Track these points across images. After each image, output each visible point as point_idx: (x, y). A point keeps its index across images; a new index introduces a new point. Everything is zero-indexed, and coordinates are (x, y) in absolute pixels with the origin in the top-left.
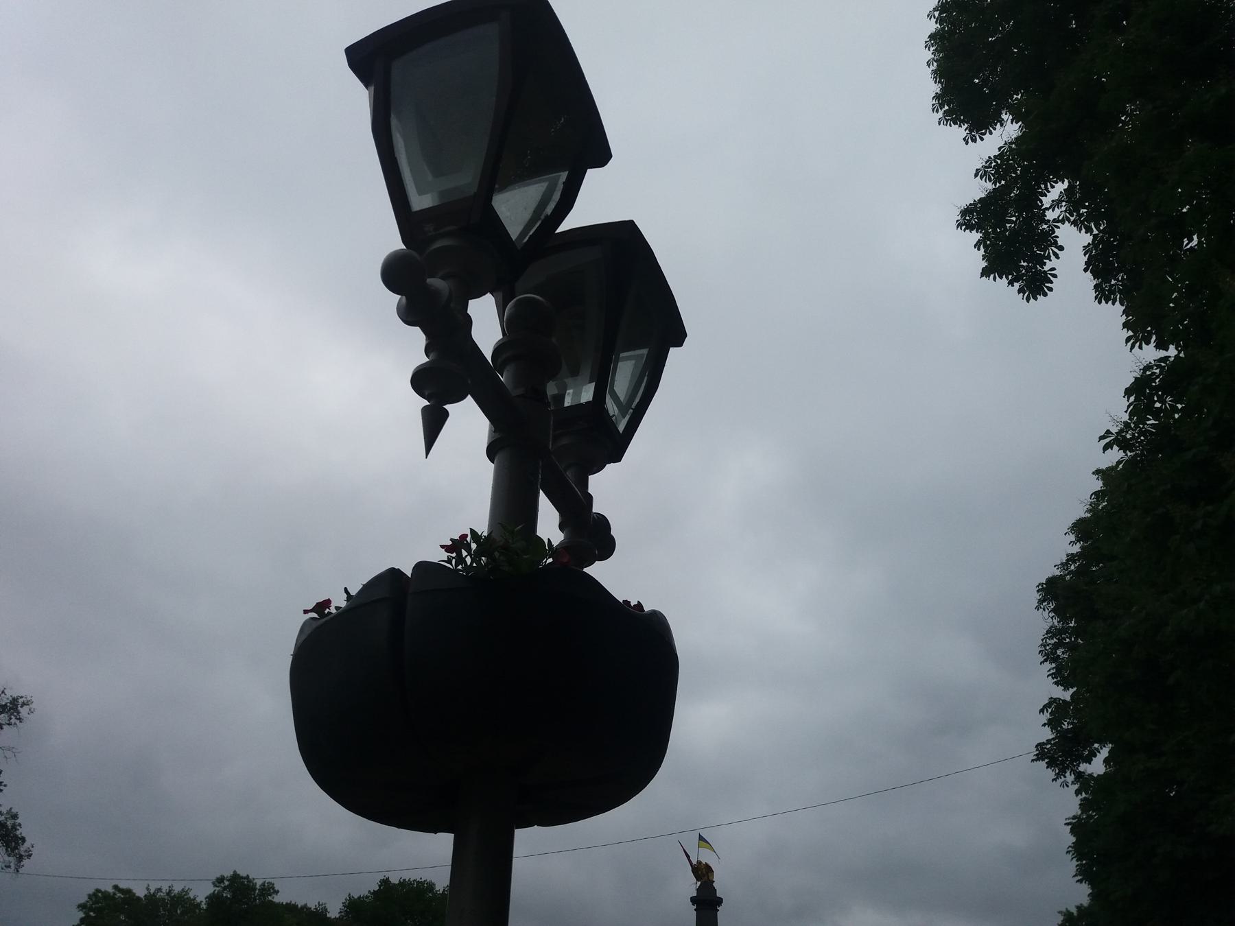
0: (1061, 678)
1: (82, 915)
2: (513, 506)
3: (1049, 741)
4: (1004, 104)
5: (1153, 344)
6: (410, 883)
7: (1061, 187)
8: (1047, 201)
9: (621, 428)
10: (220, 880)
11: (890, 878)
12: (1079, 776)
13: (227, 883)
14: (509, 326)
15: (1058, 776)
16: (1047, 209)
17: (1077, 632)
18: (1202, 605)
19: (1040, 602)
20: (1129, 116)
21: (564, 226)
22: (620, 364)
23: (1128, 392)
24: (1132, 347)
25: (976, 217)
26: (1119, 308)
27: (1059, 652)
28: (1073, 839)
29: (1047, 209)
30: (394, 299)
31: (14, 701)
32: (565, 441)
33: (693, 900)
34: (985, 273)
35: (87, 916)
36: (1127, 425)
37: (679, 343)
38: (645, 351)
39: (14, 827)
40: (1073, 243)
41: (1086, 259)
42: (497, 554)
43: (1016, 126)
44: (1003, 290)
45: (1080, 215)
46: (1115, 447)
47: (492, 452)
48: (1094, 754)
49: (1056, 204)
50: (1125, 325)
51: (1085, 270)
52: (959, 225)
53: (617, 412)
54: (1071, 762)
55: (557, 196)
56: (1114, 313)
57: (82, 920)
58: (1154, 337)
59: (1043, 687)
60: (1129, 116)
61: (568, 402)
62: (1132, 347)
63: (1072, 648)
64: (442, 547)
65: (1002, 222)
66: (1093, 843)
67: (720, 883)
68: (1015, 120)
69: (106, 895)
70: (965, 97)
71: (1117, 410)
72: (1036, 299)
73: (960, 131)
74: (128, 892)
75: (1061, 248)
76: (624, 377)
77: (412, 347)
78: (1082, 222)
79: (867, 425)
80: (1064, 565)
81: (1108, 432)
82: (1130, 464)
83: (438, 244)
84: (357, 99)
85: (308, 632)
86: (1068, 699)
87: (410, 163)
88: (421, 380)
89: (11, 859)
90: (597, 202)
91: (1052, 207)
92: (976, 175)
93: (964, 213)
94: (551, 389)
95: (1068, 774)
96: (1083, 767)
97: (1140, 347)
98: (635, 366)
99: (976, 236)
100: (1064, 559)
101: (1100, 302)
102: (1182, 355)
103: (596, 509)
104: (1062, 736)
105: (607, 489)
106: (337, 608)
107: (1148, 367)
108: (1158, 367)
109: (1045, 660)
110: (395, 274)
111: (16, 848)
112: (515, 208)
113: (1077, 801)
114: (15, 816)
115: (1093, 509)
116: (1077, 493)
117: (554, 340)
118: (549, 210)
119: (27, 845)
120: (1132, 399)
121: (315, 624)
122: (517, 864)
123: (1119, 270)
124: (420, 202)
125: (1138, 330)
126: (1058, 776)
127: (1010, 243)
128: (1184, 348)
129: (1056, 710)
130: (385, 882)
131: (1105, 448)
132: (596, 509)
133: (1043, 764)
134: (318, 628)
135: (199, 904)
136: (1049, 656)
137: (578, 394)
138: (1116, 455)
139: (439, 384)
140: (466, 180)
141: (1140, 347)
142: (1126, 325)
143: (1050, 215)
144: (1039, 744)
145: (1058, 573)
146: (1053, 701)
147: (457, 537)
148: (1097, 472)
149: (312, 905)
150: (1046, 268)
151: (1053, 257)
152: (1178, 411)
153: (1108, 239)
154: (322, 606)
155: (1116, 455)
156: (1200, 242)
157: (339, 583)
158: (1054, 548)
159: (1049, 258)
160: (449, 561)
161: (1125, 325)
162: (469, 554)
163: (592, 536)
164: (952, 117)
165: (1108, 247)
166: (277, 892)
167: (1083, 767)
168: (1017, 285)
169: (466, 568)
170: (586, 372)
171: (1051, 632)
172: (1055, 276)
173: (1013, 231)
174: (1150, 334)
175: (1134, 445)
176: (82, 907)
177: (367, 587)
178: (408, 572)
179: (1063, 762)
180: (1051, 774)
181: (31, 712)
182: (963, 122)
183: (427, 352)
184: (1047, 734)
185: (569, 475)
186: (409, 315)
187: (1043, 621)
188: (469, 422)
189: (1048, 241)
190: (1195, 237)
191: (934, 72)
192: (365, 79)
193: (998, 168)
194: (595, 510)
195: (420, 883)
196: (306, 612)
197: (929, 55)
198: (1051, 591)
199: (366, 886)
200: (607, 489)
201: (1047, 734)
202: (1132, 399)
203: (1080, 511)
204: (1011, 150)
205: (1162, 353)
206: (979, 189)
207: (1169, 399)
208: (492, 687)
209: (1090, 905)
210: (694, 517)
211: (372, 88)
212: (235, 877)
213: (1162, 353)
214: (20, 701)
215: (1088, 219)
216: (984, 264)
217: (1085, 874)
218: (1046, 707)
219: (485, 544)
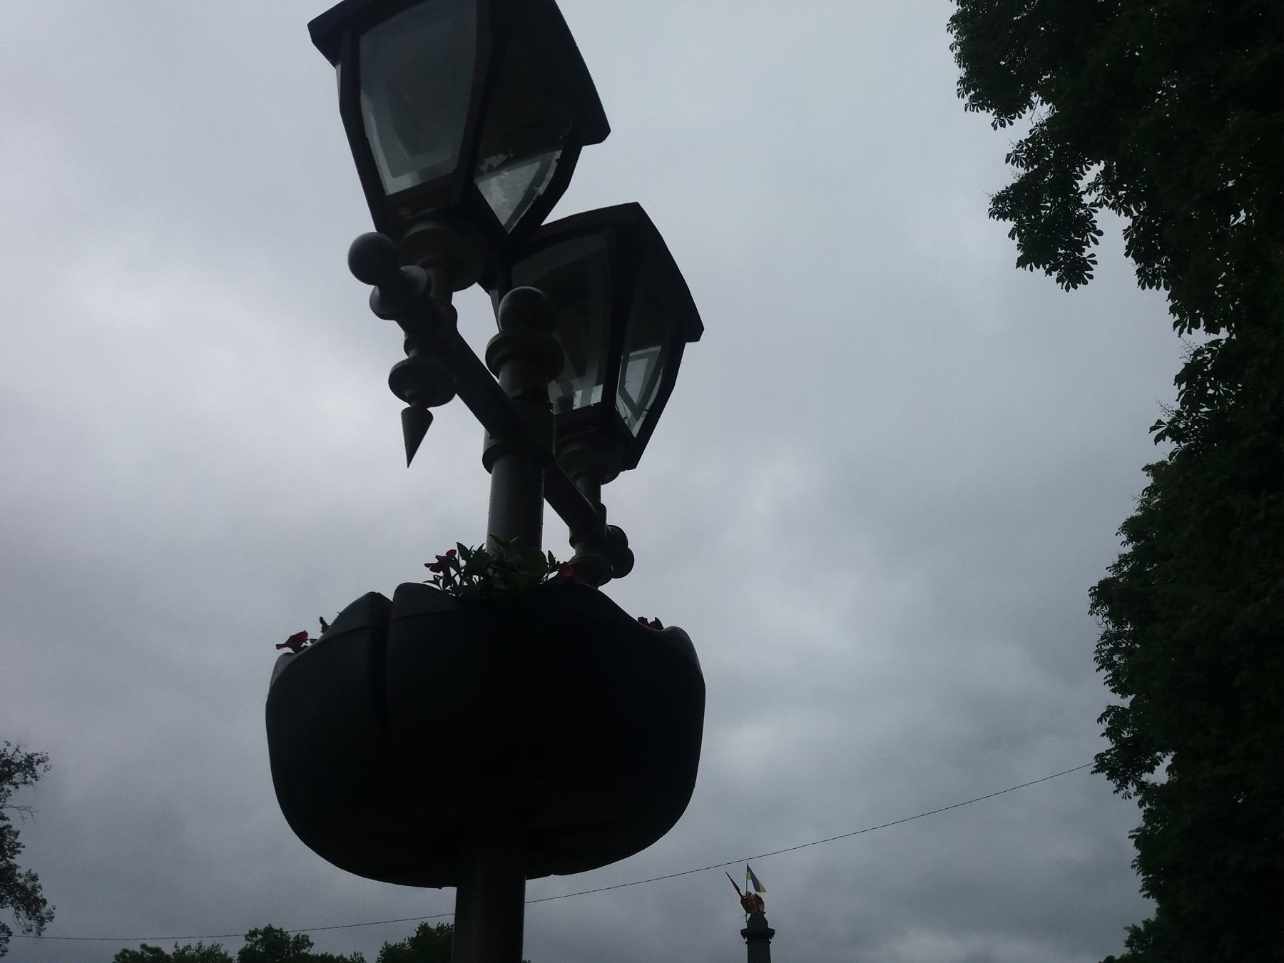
0: (1119, 684)
2: (515, 519)
3: (1108, 752)
4: (1032, 86)
5: (1202, 327)
7: (1097, 169)
8: (1082, 184)
9: (635, 432)
10: (253, 934)
11: (951, 900)
12: (1142, 786)
13: (260, 937)
14: (505, 320)
15: (1120, 787)
16: (1084, 193)
17: (1133, 636)
19: (1093, 606)
20: (1168, 88)
21: (558, 213)
22: (630, 364)
23: (1179, 379)
24: (1181, 332)
26: (1164, 293)
27: (1115, 658)
28: (1139, 853)
29: (1084, 193)
30: (366, 291)
31: (29, 758)
32: (572, 448)
33: (744, 933)
34: (1021, 263)
36: (1179, 414)
38: (658, 348)
39: (34, 889)
40: (1112, 225)
42: (490, 571)
43: (1046, 107)
44: (1041, 280)
45: (1119, 198)
46: (1168, 439)
48: (1156, 762)
49: (1092, 187)
51: (1127, 255)
52: (992, 214)
53: (629, 414)
54: (1133, 773)
56: (1159, 298)
59: (1101, 695)
60: (1168, 88)
61: (577, 404)
62: (1181, 332)
63: (1128, 653)
64: (427, 565)
65: (1036, 209)
66: (1159, 856)
69: (134, 955)
70: (992, 79)
71: (1169, 398)
73: (988, 116)
74: (157, 950)
75: (1100, 233)
76: (635, 375)
77: (389, 343)
78: (1121, 205)
80: (1117, 567)
81: (1159, 422)
82: (1182, 458)
83: (414, 230)
85: (281, 669)
86: (1127, 706)
87: (386, 153)
88: (400, 381)
89: (32, 922)
90: (594, 184)
91: (1089, 191)
92: (1007, 161)
93: (998, 200)
94: (554, 392)
95: (1130, 785)
96: (1146, 777)
97: (1190, 332)
98: (648, 366)
99: (1010, 224)
100: (1116, 561)
101: (1143, 288)
102: (1234, 337)
103: (610, 521)
104: (1121, 745)
105: (622, 499)
106: (312, 641)
107: (1199, 352)
108: (1210, 351)
109: (1101, 667)
111: (37, 910)
112: (502, 193)
113: (1140, 812)
114: (34, 878)
116: (1128, 493)
118: (541, 190)
119: (49, 906)
120: (1183, 386)
121: (292, 658)
123: (1162, 253)
124: (395, 184)
125: (1188, 311)
126: (1120, 787)
127: (1046, 231)
128: (1236, 331)
129: (1115, 720)
130: (424, 928)
131: (1157, 440)
132: (610, 521)
136: (1105, 663)
137: (586, 396)
138: (1169, 446)
140: (445, 157)
141: (1190, 332)
143: (1087, 199)
145: (1110, 575)
146: (1111, 709)
147: (443, 554)
148: (1147, 468)
150: (1085, 255)
151: (1092, 243)
153: (1149, 221)
154: (297, 640)
155: (1169, 446)
156: (1247, 218)
157: (317, 608)
158: (1106, 549)
159: (1087, 244)
160: (436, 581)
162: (459, 573)
163: (607, 551)
164: (979, 102)
167: (1146, 777)
168: (1055, 274)
169: (457, 588)
170: (593, 373)
171: (1107, 638)
172: (1095, 262)
173: (1047, 217)
175: (1187, 435)
177: (343, 616)
178: (390, 595)
179: (1124, 773)
180: (1112, 785)
182: (991, 106)
183: (407, 348)
184: (1106, 744)
185: (579, 485)
186: (383, 308)
187: (1097, 626)
188: (458, 428)
189: (1085, 226)
190: (1243, 213)
191: (958, 56)
192: (332, 56)
193: (1029, 152)
196: (279, 647)
197: (951, 38)
198: (1104, 594)
200: (622, 499)
201: (1106, 744)
202: (1183, 386)
203: (1131, 508)
205: (1213, 337)
206: (1011, 175)
208: (494, 720)
210: (714, 527)
211: (339, 67)
212: (269, 930)
213: (1213, 337)
214: (36, 758)
215: (1128, 201)
216: (1020, 254)
217: (1151, 888)
219: (476, 560)
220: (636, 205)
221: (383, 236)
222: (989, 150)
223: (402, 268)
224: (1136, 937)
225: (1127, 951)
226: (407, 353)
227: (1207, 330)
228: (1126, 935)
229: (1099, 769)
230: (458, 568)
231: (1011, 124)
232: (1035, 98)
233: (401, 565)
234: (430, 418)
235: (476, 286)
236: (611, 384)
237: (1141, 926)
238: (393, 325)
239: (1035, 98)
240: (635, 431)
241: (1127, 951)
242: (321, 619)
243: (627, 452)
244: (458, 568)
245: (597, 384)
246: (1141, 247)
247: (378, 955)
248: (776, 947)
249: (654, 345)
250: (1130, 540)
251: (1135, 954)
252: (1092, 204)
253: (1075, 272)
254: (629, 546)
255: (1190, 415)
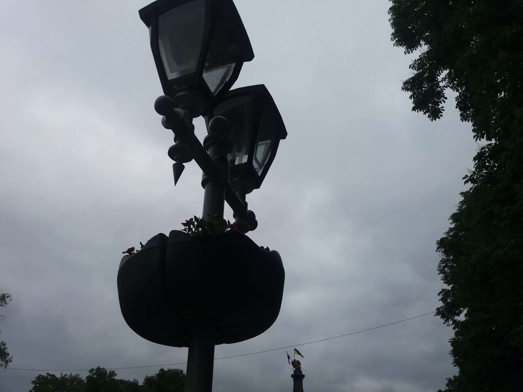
1: (33, 386)
2: (213, 206)
3: (442, 307)
5: (485, 138)
6: (173, 370)
7: (446, 72)
9: (260, 174)
10: (92, 370)
11: (377, 366)
12: (455, 322)
13: (95, 371)
14: (211, 130)
15: (446, 322)
17: (453, 261)
18: (506, 248)
19: (438, 248)
20: (475, 41)
21: (233, 88)
23: (475, 159)
24: (477, 140)
25: (410, 85)
26: (471, 123)
27: (446, 269)
31: (4, 296)
32: (235, 180)
33: (292, 376)
34: (414, 109)
35: (36, 386)
36: (474, 172)
37: (284, 138)
38: (269, 141)
39: (4, 349)
40: (451, 96)
41: (456, 103)
42: (206, 227)
43: (426, 46)
44: (422, 116)
47: (204, 184)
48: (460, 312)
49: (444, 79)
50: (473, 130)
51: (456, 107)
52: (403, 89)
53: (258, 167)
55: (231, 73)
56: (469, 125)
57: (34, 388)
58: (485, 136)
59: (440, 284)
60: (475, 41)
61: (237, 163)
62: (477, 140)
63: (451, 268)
64: (182, 224)
65: (421, 87)
66: (460, 350)
67: (304, 368)
68: (426, 43)
69: (44, 377)
71: (470, 166)
72: (435, 120)
73: (403, 49)
74: (53, 375)
75: (446, 98)
76: (260, 152)
77: (169, 138)
78: (455, 87)
79: (363, 174)
80: (448, 233)
81: (466, 176)
82: (475, 189)
83: (178, 94)
84: (144, 32)
85: (124, 261)
86: (450, 289)
88: (172, 153)
89: (3, 362)
90: (248, 76)
91: (442, 81)
92: (410, 68)
93: (405, 83)
94: (229, 157)
95: (450, 321)
96: (456, 318)
97: (480, 140)
99: (410, 93)
101: (463, 121)
102: (497, 143)
103: (249, 208)
104: (447, 305)
105: (254, 200)
106: (137, 251)
107: (483, 148)
108: (488, 148)
109: (440, 273)
110: (161, 106)
111: (5, 358)
112: (212, 79)
113: (453, 332)
114: (4, 344)
115: (460, 209)
116: (453, 203)
117: (230, 136)
118: (227, 79)
119: (10, 356)
120: (476, 162)
121: (128, 258)
122: (215, 362)
123: (471, 107)
124: (171, 76)
126: (446, 322)
127: (424, 96)
128: (498, 140)
129: (445, 295)
130: (162, 370)
131: (465, 183)
132: (249, 208)
133: (439, 317)
134: (128, 260)
135: (83, 381)
136: (442, 271)
137: (241, 159)
138: (470, 185)
139: (180, 154)
140: (191, 66)
141: (480, 140)
142: (474, 131)
143: (441, 84)
144: (437, 308)
145: (445, 236)
146: (443, 290)
147: (188, 220)
148: (462, 193)
149: (131, 380)
150: (440, 107)
151: (442, 102)
152: (495, 167)
153: (466, 94)
155: (470, 185)
156: (505, 95)
157: (138, 240)
158: (444, 226)
159: (441, 102)
160: (185, 230)
161: (473, 130)
162: (194, 227)
163: (247, 220)
164: (400, 43)
165: (465, 96)
166: (116, 375)
167: (456, 318)
168: (427, 114)
169: (193, 233)
170: (244, 150)
171: (443, 261)
172: (443, 110)
173: (425, 91)
174: (484, 134)
175: (477, 181)
176: (33, 382)
177: (150, 242)
178: (168, 235)
179: (447, 316)
180: (443, 321)
181: (11, 300)
182: (404, 45)
184: (441, 304)
185: (237, 194)
186: (167, 124)
187: (439, 256)
188: (193, 171)
189: (440, 95)
190: (503, 93)
191: (392, 24)
192: (148, 23)
193: (419, 64)
194: (248, 209)
195: (177, 370)
196: (124, 253)
197: (389, 17)
198: (442, 244)
199: (154, 372)
200: (254, 200)
201: (441, 304)
202: (476, 162)
204: (424, 56)
205: (489, 142)
206: (411, 73)
207: (492, 161)
208: (204, 284)
209: (459, 376)
210: (284, 211)
211: (150, 28)
212: (99, 369)
213: (489, 142)
214: (6, 295)
215: (457, 86)
216: (413, 105)
217: (457, 363)
218: (440, 293)
219: (201, 223)
220: (263, 85)
221: (168, 97)
222: (403, 63)
223: (175, 109)
224: (450, 382)
225: (447, 388)
226: (175, 142)
227: (487, 139)
228: (447, 382)
229: (438, 314)
230: (194, 225)
231: (412, 52)
232: (422, 43)
233: (171, 223)
234: (183, 167)
235: (201, 116)
236: (251, 155)
237: (452, 378)
238: (170, 131)
239: (422, 43)
240: (260, 174)
241: (447, 388)
242: (141, 243)
243: (256, 182)
244: (194, 225)
245: (246, 154)
246: (462, 104)
247: (143, 381)
248: (306, 383)
249: (268, 140)
250: (454, 222)
251: (450, 389)
252: (443, 87)
253: (435, 114)
254: (256, 219)
255: (478, 173)
